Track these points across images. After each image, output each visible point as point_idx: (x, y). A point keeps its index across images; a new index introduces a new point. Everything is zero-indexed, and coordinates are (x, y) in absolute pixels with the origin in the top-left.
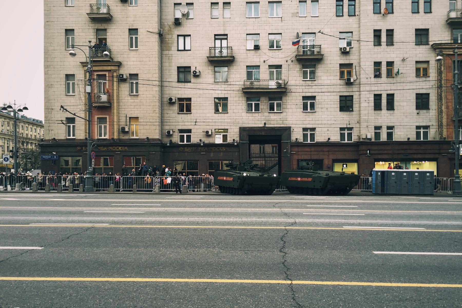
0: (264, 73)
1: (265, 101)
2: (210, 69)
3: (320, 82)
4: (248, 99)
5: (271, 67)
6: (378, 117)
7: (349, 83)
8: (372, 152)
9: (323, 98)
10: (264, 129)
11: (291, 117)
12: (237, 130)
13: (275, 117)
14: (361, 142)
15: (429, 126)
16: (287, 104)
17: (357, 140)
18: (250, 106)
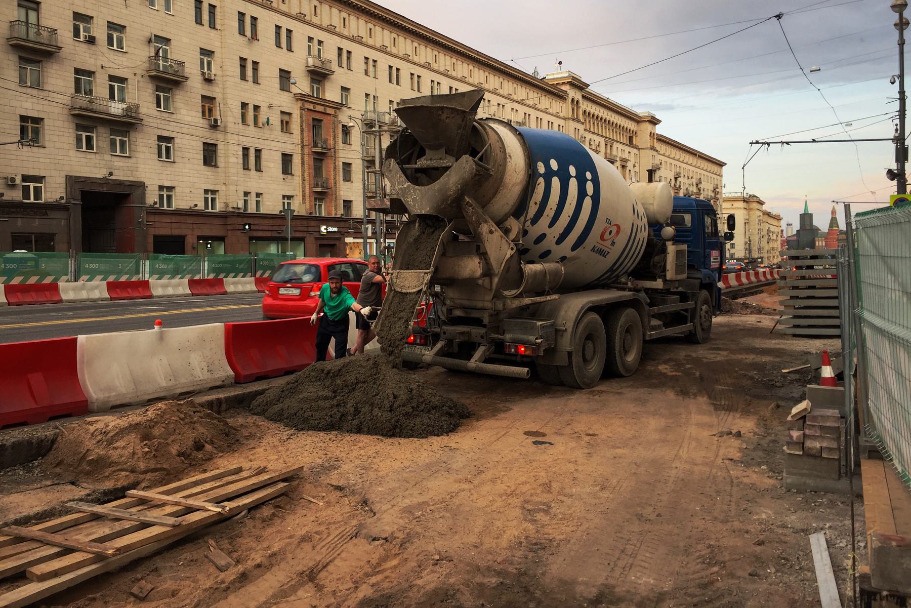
0: (101, 88)
1: (104, 135)
2: (11, 58)
3: (179, 117)
4: (79, 127)
5: (112, 78)
6: (247, 180)
7: (214, 126)
8: (252, 227)
9: (185, 142)
10: (104, 181)
11: (142, 166)
12: (62, 181)
13: (121, 164)
14: (229, 212)
15: (293, 196)
16: (137, 144)
17: (224, 210)
18: (79, 139)
